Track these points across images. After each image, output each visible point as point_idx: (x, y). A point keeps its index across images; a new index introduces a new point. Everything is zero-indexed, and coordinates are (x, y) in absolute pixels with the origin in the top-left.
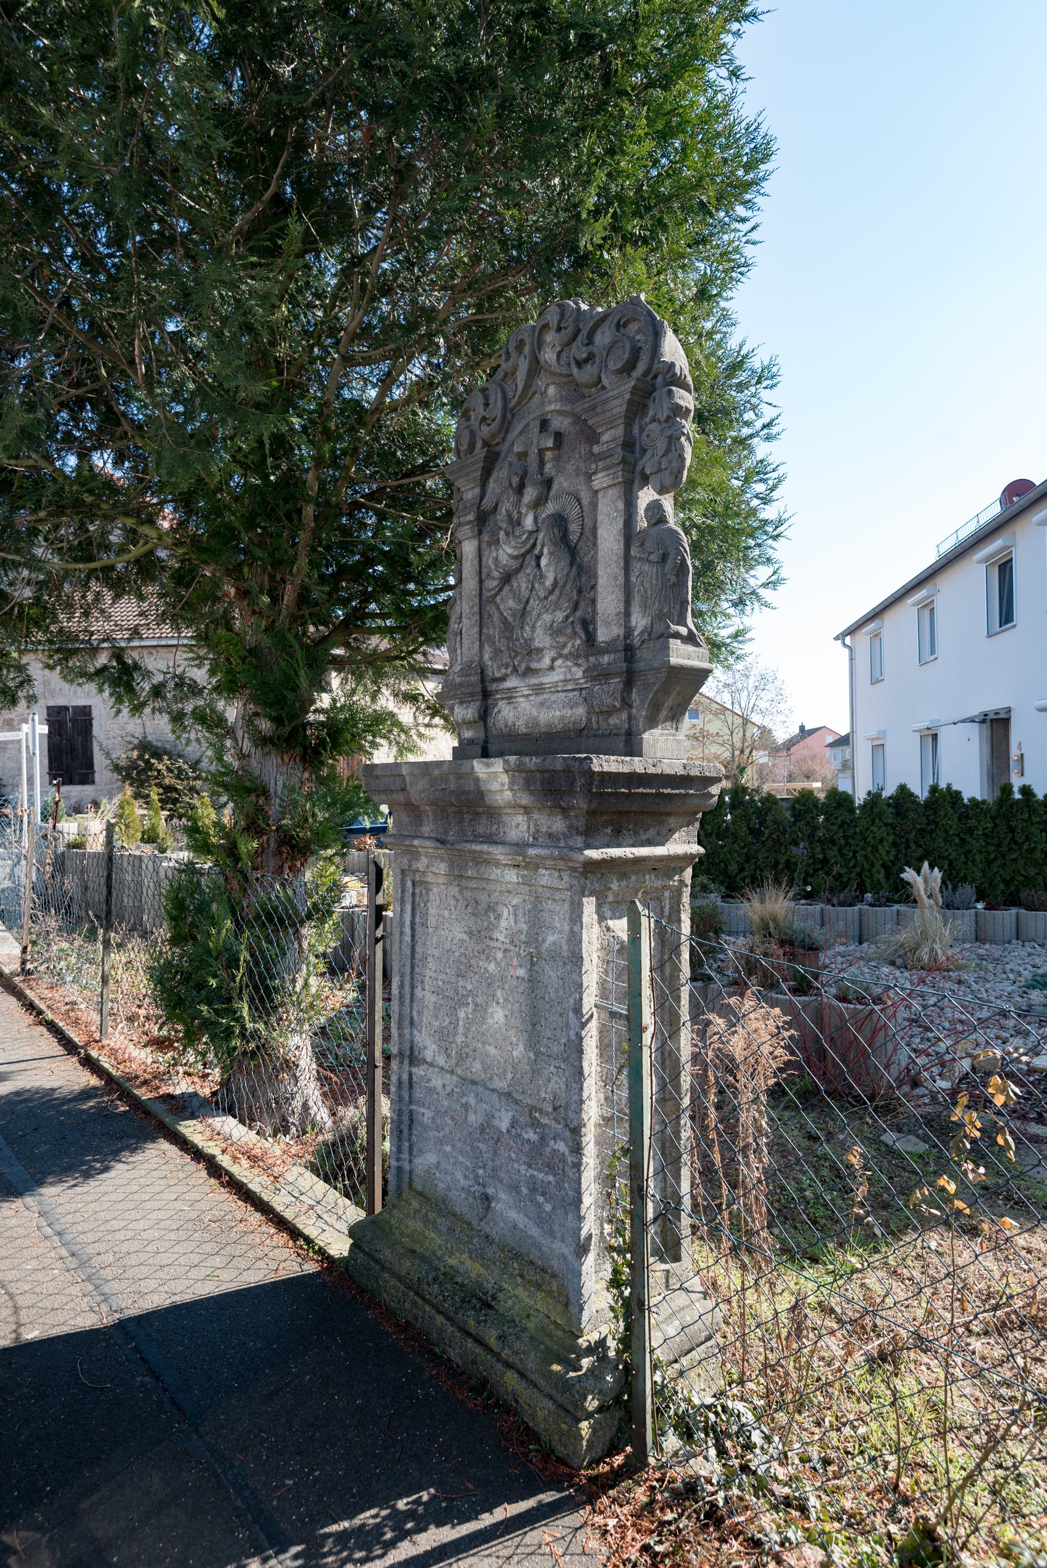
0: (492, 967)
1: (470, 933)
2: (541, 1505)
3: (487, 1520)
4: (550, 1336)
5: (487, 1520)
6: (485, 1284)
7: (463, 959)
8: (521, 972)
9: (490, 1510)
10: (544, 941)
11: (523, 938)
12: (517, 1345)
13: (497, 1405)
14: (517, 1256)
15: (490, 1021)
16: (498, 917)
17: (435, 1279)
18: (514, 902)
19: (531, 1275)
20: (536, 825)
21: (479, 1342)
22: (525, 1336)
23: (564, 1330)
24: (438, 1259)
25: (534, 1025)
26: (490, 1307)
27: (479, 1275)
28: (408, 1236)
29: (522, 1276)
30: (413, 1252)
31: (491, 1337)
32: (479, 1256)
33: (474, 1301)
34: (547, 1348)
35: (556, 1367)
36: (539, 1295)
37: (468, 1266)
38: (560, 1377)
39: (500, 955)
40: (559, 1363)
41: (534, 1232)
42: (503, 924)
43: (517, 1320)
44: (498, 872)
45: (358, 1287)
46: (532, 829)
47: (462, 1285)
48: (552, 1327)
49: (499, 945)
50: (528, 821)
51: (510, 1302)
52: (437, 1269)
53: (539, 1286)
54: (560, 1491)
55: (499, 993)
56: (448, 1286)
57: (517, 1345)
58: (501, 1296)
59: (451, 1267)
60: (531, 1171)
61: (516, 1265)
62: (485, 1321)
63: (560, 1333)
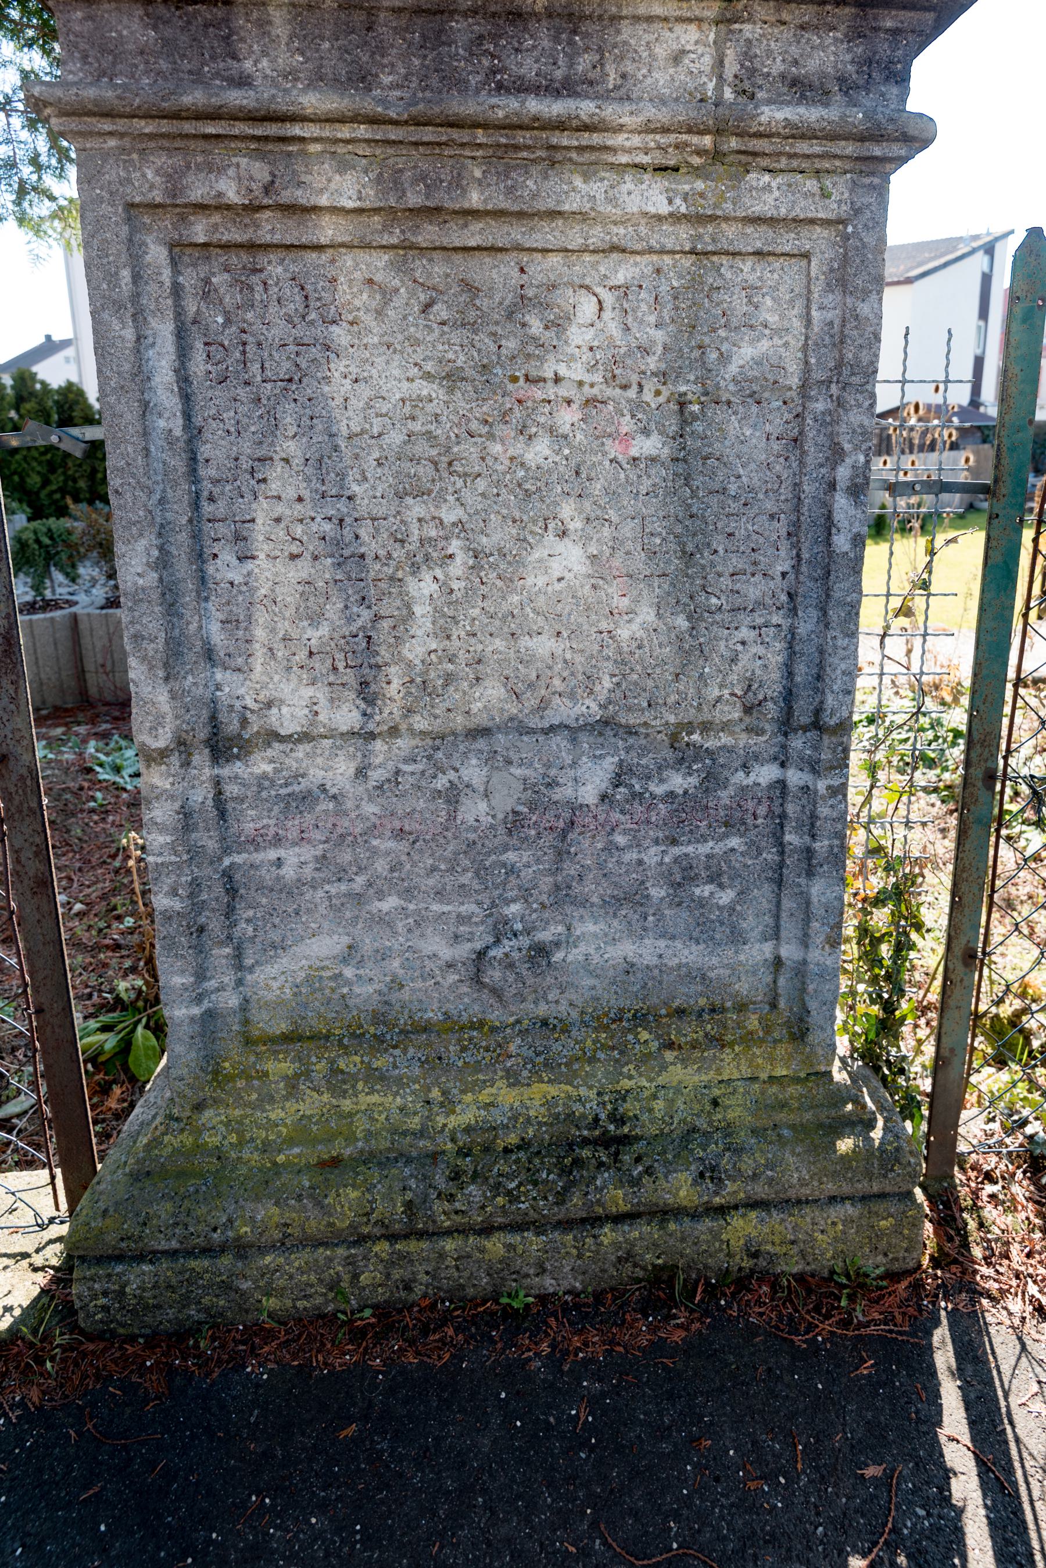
0: (539, 451)
1: (452, 378)
2: (960, 1372)
3: (966, 1488)
4: (783, 1105)
5: (966, 1488)
6: (578, 1109)
7: (421, 448)
8: (650, 445)
9: (947, 1474)
10: (724, 359)
11: (652, 363)
12: (747, 1164)
13: (712, 1291)
14: (640, 1019)
15: (535, 580)
16: (558, 325)
17: (456, 1176)
18: (620, 277)
19: (689, 1031)
20: (747, 56)
21: (663, 1214)
22: (742, 1137)
23: (796, 1080)
24: (422, 1134)
25: (688, 557)
26: (626, 1140)
27: (549, 1103)
28: (291, 1142)
29: (671, 1046)
30: (335, 1162)
31: (681, 1187)
32: (545, 1066)
33: (586, 1153)
34: (793, 1127)
35: (845, 1145)
36: (727, 1055)
37: (517, 1101)
38: (866, 1154)
39: (567, 418)
40: (841, 1136)
41: (688, 954)
42: (578, 336)
43: (702, 1123)
44: (597, 188)
45: (153, 1341)
46: (731, 68)
47: (524, 1145)
48: (774, 1089)
49: (563, 391)
50: (719, 45)
51: (659, 1105)
52: (434, 1156)
53: (719, 1042)
54: (937, 1323)
55: (567, 510)
56: (501, 1166)
57: (747, 1164)
58: (630, 1107)
59: (468, 1130)
60: (676, 851)
61: (645, 1035)
62: (649, 1171)
63: (793, 1090)
